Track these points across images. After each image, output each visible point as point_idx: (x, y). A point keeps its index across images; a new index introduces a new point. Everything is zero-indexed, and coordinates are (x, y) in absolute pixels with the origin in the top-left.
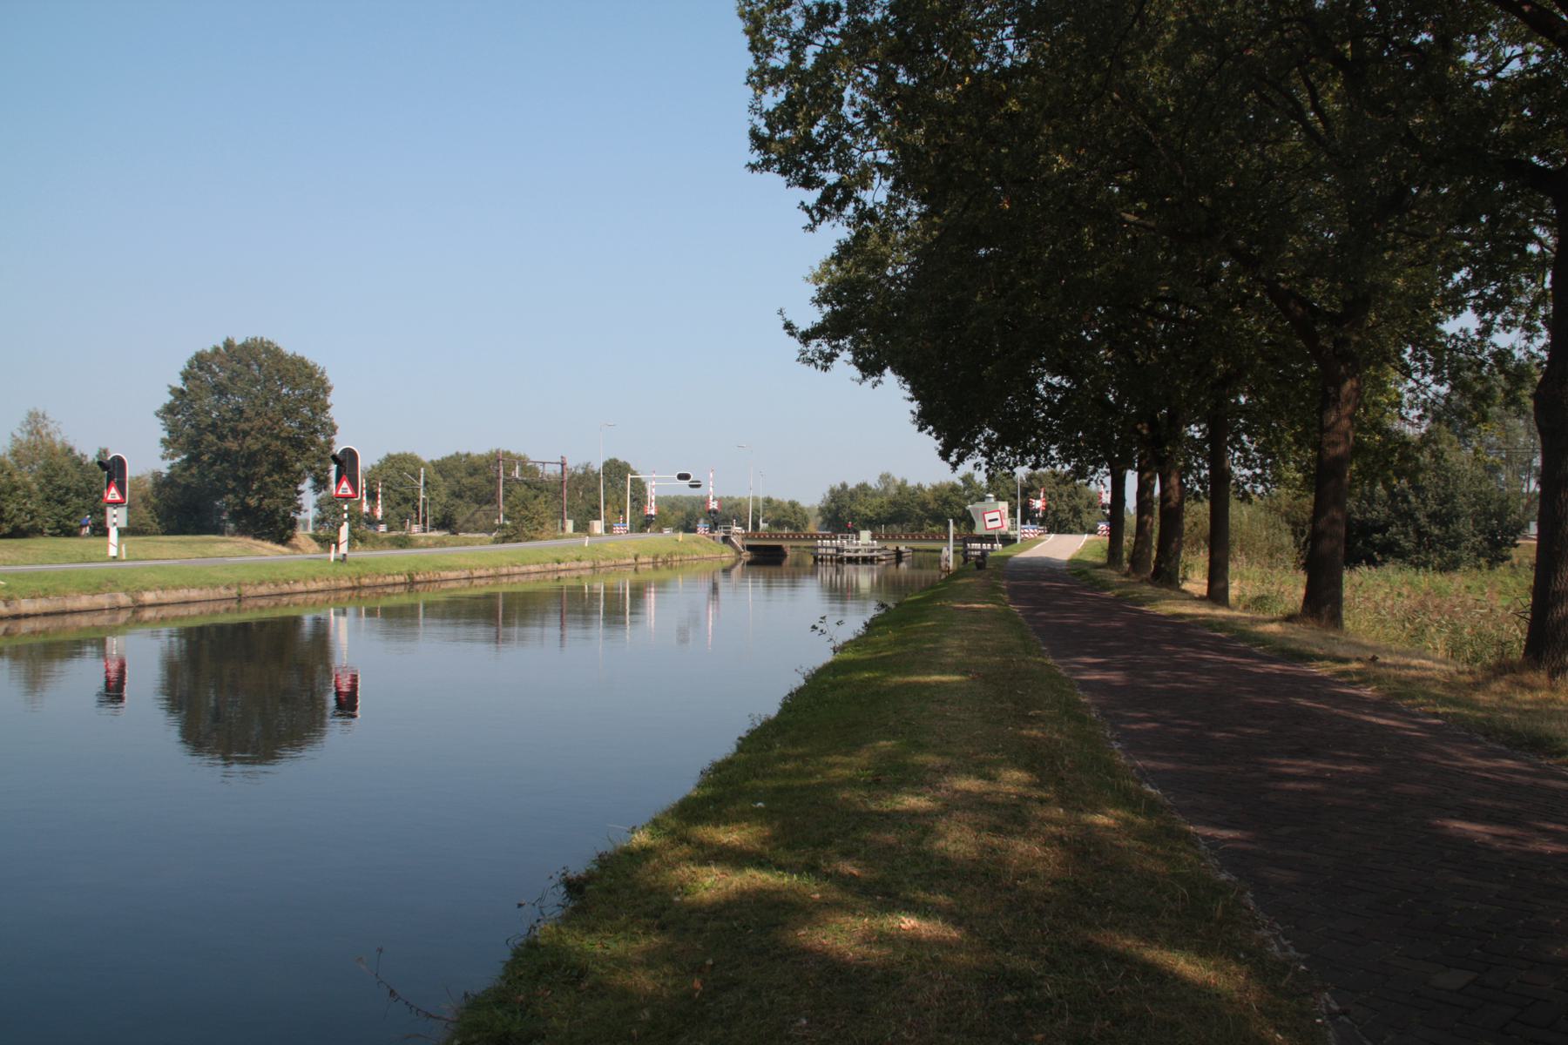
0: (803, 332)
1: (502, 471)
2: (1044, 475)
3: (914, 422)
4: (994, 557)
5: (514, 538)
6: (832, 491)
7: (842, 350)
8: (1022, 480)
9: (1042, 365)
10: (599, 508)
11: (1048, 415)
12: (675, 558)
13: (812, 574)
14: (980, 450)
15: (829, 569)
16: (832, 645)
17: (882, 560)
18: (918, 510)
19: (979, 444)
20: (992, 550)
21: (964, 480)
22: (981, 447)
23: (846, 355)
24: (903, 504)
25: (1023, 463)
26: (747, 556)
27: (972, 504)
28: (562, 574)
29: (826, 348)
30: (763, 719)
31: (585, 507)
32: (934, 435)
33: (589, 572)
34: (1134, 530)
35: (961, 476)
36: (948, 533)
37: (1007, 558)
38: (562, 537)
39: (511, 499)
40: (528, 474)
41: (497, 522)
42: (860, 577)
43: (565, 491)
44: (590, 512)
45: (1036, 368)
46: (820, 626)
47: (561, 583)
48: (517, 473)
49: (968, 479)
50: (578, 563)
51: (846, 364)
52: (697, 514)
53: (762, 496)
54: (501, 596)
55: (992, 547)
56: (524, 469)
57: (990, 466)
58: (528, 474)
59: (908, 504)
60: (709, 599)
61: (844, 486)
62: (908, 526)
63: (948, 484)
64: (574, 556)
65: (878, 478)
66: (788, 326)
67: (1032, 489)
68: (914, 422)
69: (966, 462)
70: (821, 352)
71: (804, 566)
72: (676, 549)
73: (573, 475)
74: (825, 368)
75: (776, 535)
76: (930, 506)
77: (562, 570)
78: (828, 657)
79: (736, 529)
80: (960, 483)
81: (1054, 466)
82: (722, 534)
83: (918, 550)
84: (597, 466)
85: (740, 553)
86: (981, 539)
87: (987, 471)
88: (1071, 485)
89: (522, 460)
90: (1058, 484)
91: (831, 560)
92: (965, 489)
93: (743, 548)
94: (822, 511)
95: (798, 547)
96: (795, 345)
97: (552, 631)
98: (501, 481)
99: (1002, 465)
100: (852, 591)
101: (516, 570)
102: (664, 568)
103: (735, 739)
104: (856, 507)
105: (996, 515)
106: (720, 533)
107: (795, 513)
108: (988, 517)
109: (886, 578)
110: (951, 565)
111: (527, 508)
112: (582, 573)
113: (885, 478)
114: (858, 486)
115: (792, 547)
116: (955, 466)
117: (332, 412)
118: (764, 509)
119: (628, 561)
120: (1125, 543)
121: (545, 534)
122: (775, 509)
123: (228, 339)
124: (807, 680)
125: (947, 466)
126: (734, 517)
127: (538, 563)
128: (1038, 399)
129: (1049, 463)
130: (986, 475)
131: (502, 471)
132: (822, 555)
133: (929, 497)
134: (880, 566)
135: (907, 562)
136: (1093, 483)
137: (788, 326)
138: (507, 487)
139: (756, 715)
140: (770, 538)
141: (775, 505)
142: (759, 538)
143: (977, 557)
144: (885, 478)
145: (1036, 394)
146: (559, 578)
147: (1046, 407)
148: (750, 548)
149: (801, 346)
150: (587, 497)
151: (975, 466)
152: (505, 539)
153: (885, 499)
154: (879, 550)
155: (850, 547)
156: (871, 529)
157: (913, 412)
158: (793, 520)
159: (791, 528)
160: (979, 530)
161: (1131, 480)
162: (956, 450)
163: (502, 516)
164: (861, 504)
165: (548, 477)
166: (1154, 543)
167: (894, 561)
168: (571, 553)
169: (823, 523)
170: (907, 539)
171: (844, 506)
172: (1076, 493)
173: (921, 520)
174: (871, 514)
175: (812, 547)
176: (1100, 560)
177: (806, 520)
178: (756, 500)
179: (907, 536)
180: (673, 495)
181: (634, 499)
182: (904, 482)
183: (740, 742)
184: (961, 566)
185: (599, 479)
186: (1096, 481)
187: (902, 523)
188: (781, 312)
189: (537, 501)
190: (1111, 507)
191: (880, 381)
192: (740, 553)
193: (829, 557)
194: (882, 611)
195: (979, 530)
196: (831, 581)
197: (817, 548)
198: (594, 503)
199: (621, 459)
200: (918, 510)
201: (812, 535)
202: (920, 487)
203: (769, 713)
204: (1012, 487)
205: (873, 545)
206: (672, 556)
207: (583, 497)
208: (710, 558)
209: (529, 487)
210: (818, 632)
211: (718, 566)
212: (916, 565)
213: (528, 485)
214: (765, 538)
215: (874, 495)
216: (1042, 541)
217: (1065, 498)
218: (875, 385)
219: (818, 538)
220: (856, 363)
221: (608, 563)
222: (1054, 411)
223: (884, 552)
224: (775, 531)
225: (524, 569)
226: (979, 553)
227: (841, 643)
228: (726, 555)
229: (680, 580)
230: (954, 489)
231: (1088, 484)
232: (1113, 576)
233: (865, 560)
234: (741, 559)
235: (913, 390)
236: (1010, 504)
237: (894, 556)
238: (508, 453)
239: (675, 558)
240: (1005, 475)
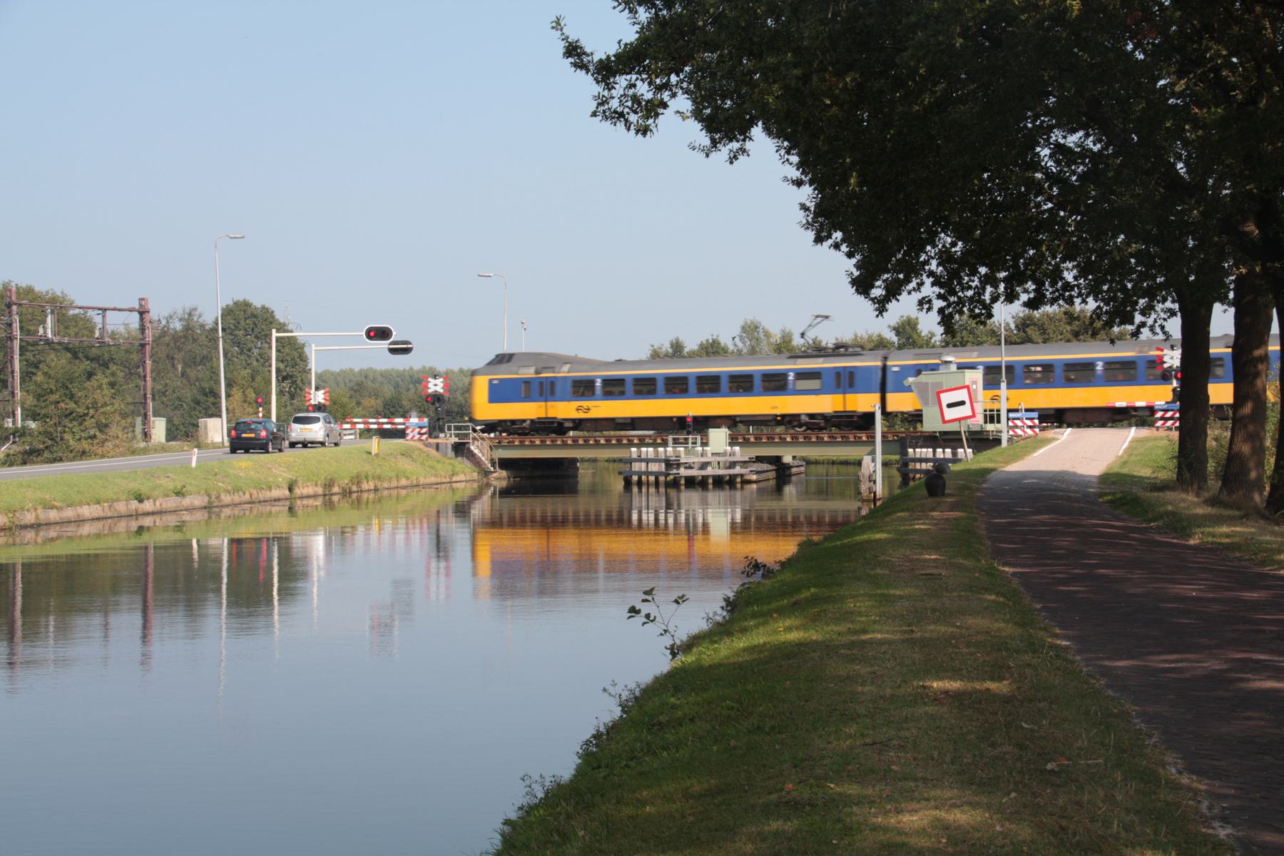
1: (16, 326)
2: (1051, 318)
3: (808, 225)
4: (959, 473)
5: (47, 454)
8: (1007, 328)
9: (1048, 112)
10: (217, 396)
11: (1060, 205)
12: (365, 486)
14: (931, 274)
16: (668, 641)
17: (750, 482)
19: (927, 262)
20: (955, 460)
23: (682, 103)
25: (1011, 297)
26: (500, 478)
28: (147, 522)
29: (644, 91)
30: (547, 784)
31: (188, 394)
35: (894, 322)
38: (145, 451)
39: (39, 378)
40: (72, 332)
41: (9, 423)
44: (198, 403)
45: (1036, 117)
46: (645, 609)
47: (146, 538)
48: (48, 329)
50: (179, 499)
51: (750, 153)
52: (405, 403)
54: (19, 568)
55: (954, 454)
56: (64, 322)
58: (72, 332)
60: (430, 557)
64: (171, 486)
66: (573, 51)
68: (808, 225)
69: (904, 297)
70: (636, 99)
72: (367, 468)
74: (644, 131)
77: (147, 514)
80: (892, 337)
81: (1070, 301)
82: (455, 440)
83: (816, 463)
84: (210, 314)
86: (934, 440)
87: (941, 311)
89: (58, 305)
91: (657, 484)
93: (493, 464)
95: (594, 460)
96: (587, 86)
97: (126, 621)
98: (17, 344)
101: (53, 515)
102: (345, 505)
103: (498, 825)
105: (962, 395)
108: (947, 398)
110: (879, 488)
111: (72, 397)
112: (186, 517)
116: (881, 306)
119: (276, 493)
121: (109, 445)
123: (677, 339)
124: (624, 707)
125: (867, 307)
128: (1039, 175)
129: (1062, 296)
131: (16, 326)
132: (640, 474)
137: (573, 51)
138: (29, 355)
139: (536, 777)
143: (927, 472)
145: (1036, 165)
147: (1055, 191)
148: (505, 464)
149: (598, 89)
150: (192, 373)
151: (921, 303)
152: (29, 457)
154: (744, 464)
155: (691, 460)
157: (804, 207)
161: (1222, 321)
163: (19, 411)
166: (1268, 443)
167: (773, 483)
168: (163, 481)
175: (620, 460)
176: (1164, 475)
180: (357, 369)
181: (282, 378)
183: (507, 829)
185: (216, 340)
186: (1152, 328)
188: (558, 25)
189: (94, 383)
191: (743, 151)
192: (486, 473)
193: (652, 478)
196: (657, 520)
197: (630, 461)
198: (206, 385)
199: (257, 302)
203: (558, 773)
205: (732, 454)
206: (359, 483)
207: (183, 374)
208: (430, 485)
209: (75, 356)
210: (640, 619)
211: (446, 498)
212: (813, 489)
213: (74, 353)
218: (733, 159)
220: (697, 114)
222: (1069, 197)
225: (69, 513)
226: (929, 466)
227: (685, 638)
228: (461, 477)
232: (1189, 502)
234: (488, 485)
238: (29, 291)
239: (365, 486)
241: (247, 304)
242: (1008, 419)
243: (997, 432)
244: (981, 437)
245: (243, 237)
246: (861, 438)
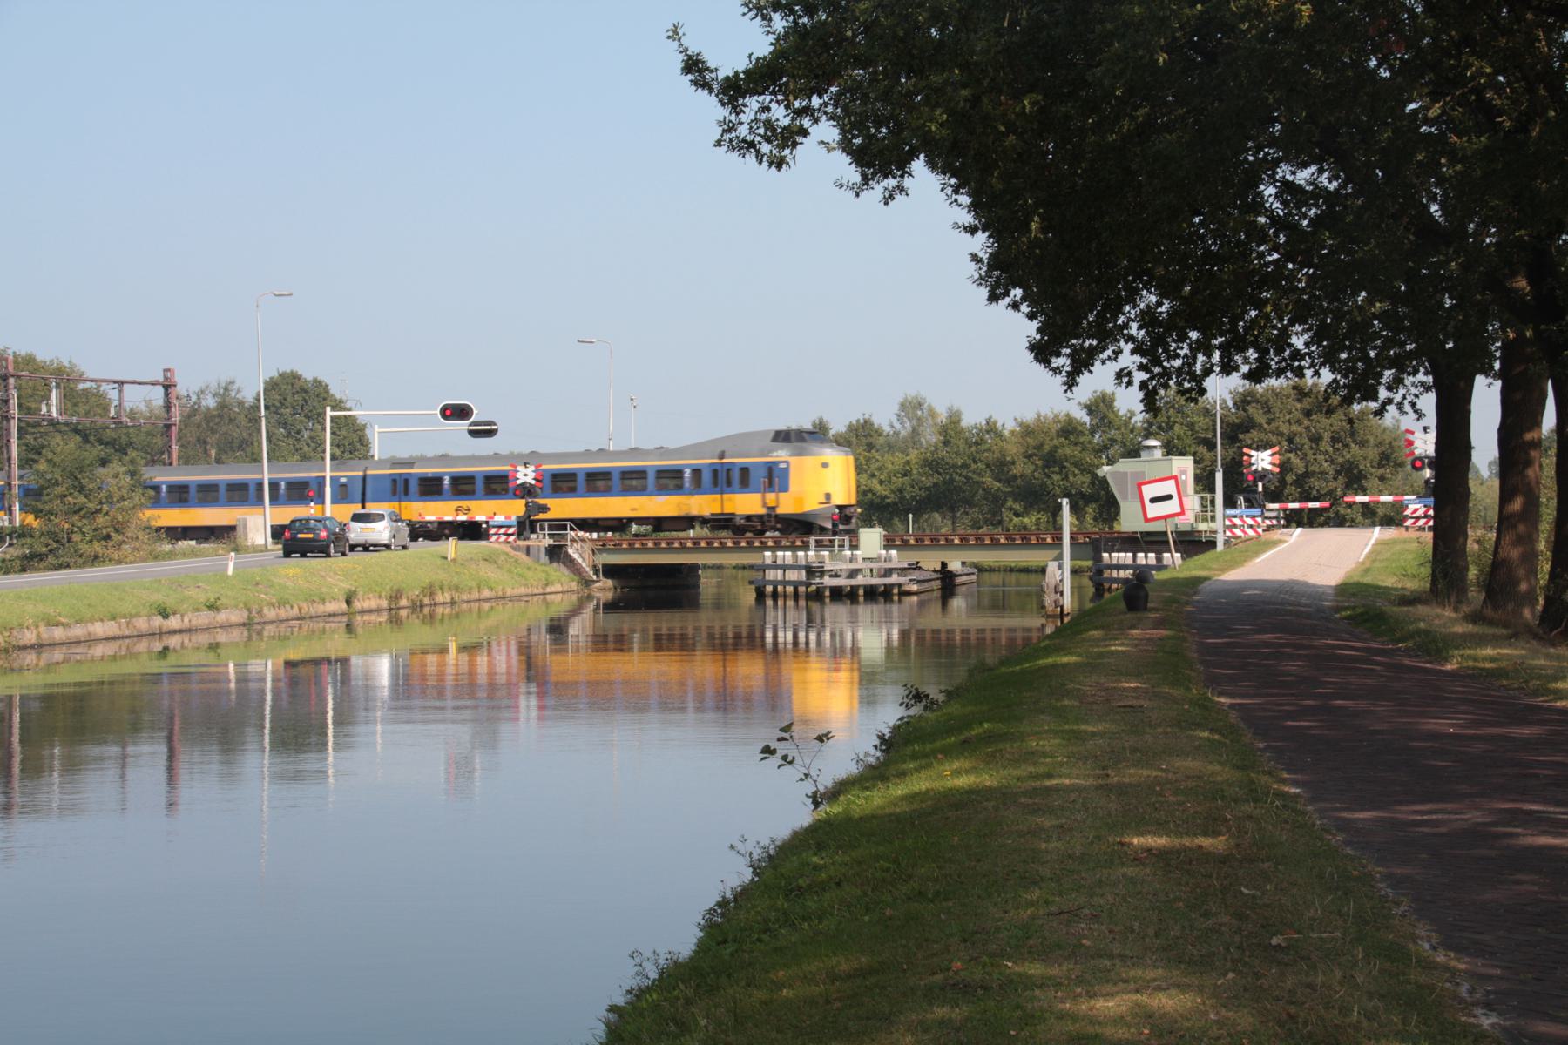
0: (727, 78)
1: (14, 402)
4: (1164, 583)
5: (51, 559)
7: (816, 121)
8: (1224, 406)
11: (1287, 256)
12: (440, 598)
15: (791, 614)
16: (811, 789)
17: (909, 593)
18: (988, 480)
20: (1160, 566)
23: (826, 131)
24: (955, 466)
25: (1228, 368)
26: (605, 589)
27: (1111, 462)
28: (174, 641)
29: (780, 115)
33: (237, 635)
34: (1493, 515)
35: (1084, 400)
37: (1195, 582)
39: (42, 466)
42: (860, 635)
43: (175, 447)
45: (1259, 148)
48: (53, 407)
49: (1100, 407)
55: (1159, 559)
56: (71, 397)
58: (82, 409)
59: (965, 466)
63: (1056, 419)
64: (202, 597)
65: (896, 408)
66: (694, 66)
67: (1247, 425)
70: (769, 125)
72: (442, 576)
73: (194, 411)
74: (779, 163)
78: (803, 816)
80: (1082, 416)
82: (549, 542)
83: (991, 570)
84: (251, 388)
85: (588, 583)
86: (1133, 542)
88: (1339, 415)
89: (65, 378)
90: (1308, 414)
92: (1092, 432)
93: (596, 571)
96: (710, 108)
98: (14, 424)
101: (59, 634)
102: (415, 621)
105: (1168, 487)
108: (1149, 491)
110: (1067, 601)
111: (81, 489)
113: (912, 408)
114: (851, 428)
116: (1071, 383)
117: (1008, 425)
119: (331, 607)
120: (1472, 546)
121: (127, 548)
127: (114, 618)
128: (1262, 220)
129: (1289, 367)
130: (1141, 395)
131: (14, 402)
132: (775, 584)
133: (1013, 450)
135: (966, 596)
136: (1392, 409)
137: (694, 66)
139: (647, 953)
143: (1126, 581)
144: (912, 408)
145: (1258, 206)
146: (166, 649)
148: (610, 571)
149: (723, 113)
151: (1119, 375)
153: (913, 455)
155: (837, 566)
156: (882, 524)
157: (975, 258)
160: (1130, 521)
161: (1486, 400)
165: (132, 414)
167: (937, 594)
168: (193, 592)
172: (1352, 434)
173: (996, 502)
176: (1411, 585)
179: (964, 539)
182: (954, 418)
183: (612, 1017)
184: (1089, 605)
185: (257, 420)
186: (1400, 406)
188: (675, 33)
190: (1434, 463)
191: (901, 189)
192: (588, 583)
193: (790, 589)
195: (1130, 521)
197: (763, 568)
199: (308, 374)
200: (988, 480)
202: (991, 428)
203: (675, 949)
204: (1202, 422)
206: (432, 594)
209: (86, 439)
210: (775, 761)
211: (539, 615)
213: (84, 435)
215: (891, 447)
216: (1281, 541)
217: (1325, 446)
218: (888, 198)
220: (846, 145)
221: (283, 614)
222: (1300, 246)
223: (916, 575)
225: (78, 631)
226: (1129, 574)
227: (830, 784)
228: (558, 588)
230: (1069, 429)
231: (1380, 412)
232: (1445, 618)
234: (590, 597)
235: (974, 207)
237: (937, 585)
238: (30, 360)
239: (440, 598)
241: (295, 377)
242: (1225, 517)
244: (1191, 539)
245: (291, 295)
246: (1045, 539)
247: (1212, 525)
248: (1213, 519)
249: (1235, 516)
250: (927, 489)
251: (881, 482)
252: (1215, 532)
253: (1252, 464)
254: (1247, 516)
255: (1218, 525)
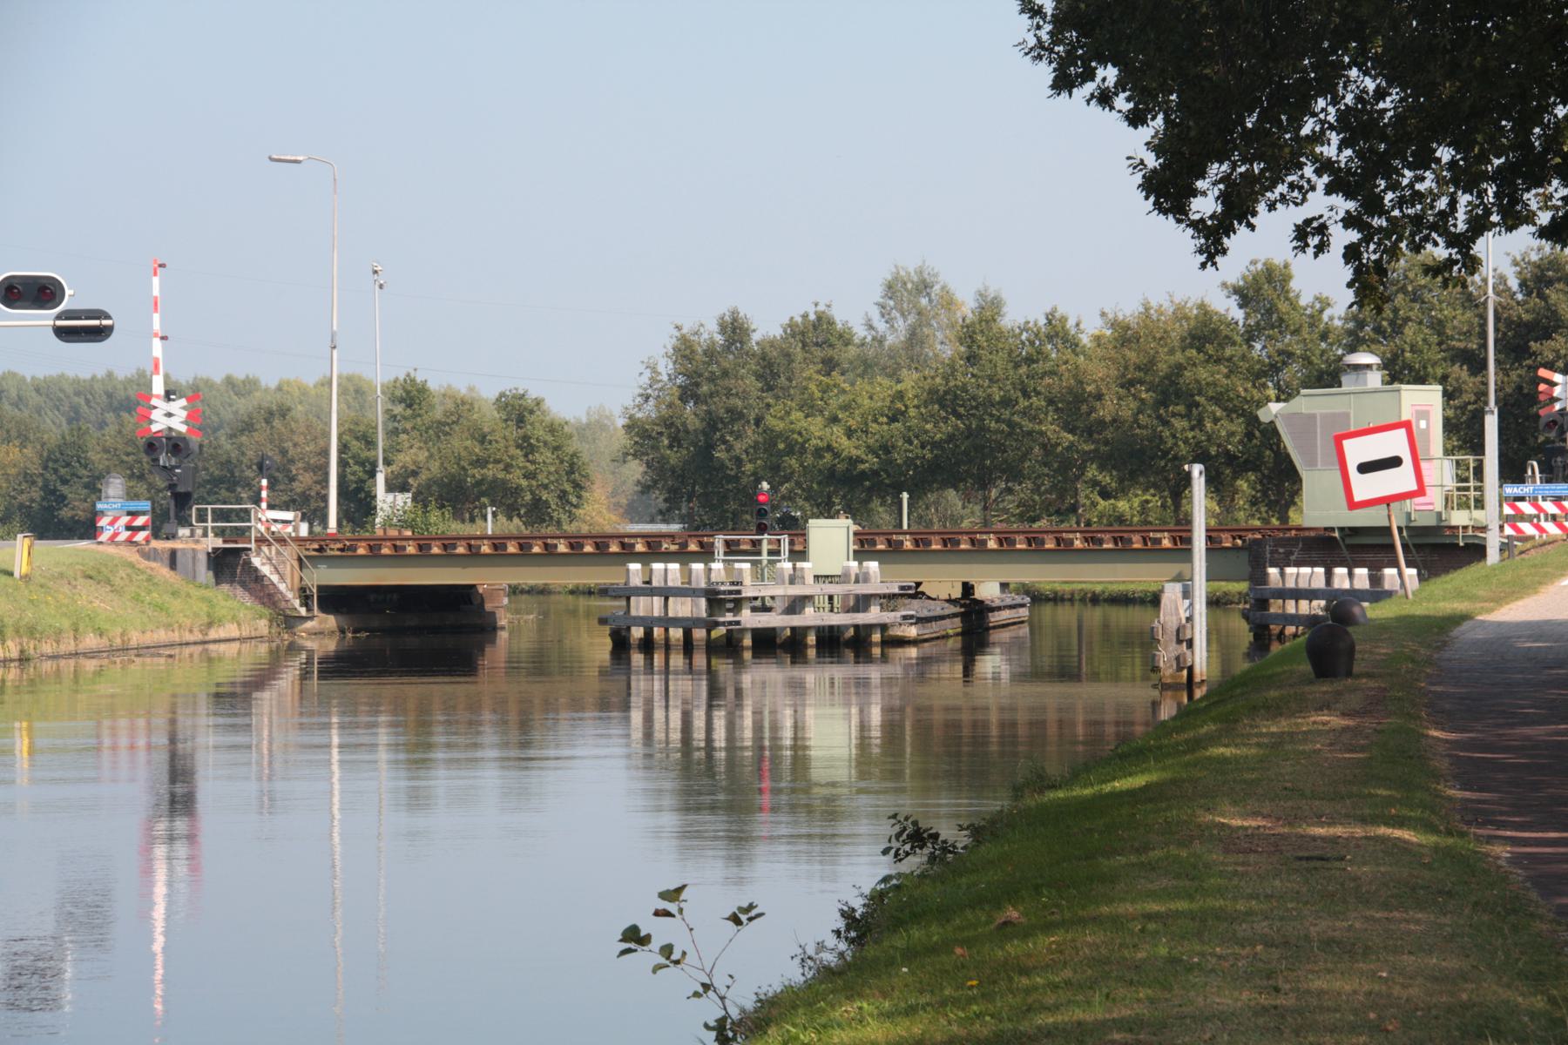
6: (685, 351)
13: (604, 705)
14: (1325, 166)
16: (710, 1010)
17: (902, 642)
18: (1051, 428)
19: (1318, 138)
20: (1377, 593)
21: (1246, 295)
22: (1330, 151)
25: (1514, 218)
32: (1122, 103)
36: (1187, 522)
37: (1441, 627)
46: (663, 929)
52: (94, 456)
53: (381, 373)
55: (1376, 580)
57: (1368, 233)
59: (1007, 402)
61: (735, 329)
62: (1009, 498)
63: (1180, 314)
65: (877, 294)
69: (1262, 216)
71: (570, 667)
75: (448, 544)
76: (1106, 411)
79: (268, 518)
83: (1056, 599)
85: (289, 621)
87: (1351, 253)
91: (688, 646)
93: (306, 600)
94: (642, 436)
95: (543, 591)
99: (1422, 228)
100: (776, 775)
104: (787, 418)
105: (1393, 443)
106: (198, 540)
107: (527, 446)
108: (1358, 450)
109: (923, 730)
110: (1200, 658)
115: (514, 591)
116: (1213, 239)
118: (393, 433)
122: (441, 429)
126: (261, 468)
130: (1347, 273)
132: (648, 624)
133: (1098, 372)
134: (894, 670)
135: (1010, 648)
140: (424, 556)
141: (438, 414)
142: (374, 556)
143: (1312, 621)
148: (333, 599)
153: (910, 381)
154: (889, 600)
156: (851, 512)
158: (516, 478)
159: (511, 511)
162: (1216, 169)
164: (809, 408)
167: (955, 644)
169: (646, 489)
170: (1006, 549)
171: (736, 415)
173: (1066, 468)
174: (847, 446)
177: (574, 477)
178: (355, 390)
179: (1005, 540)
182: (990, 309)
187: (984, 483)
193: (676, 634)
194: (914, 863)
197: (627, 594)
200: (1051, 428)
201: (601, 542)
202: (1056, 331)
204: (1461, 318)
205: (862, 578)
210: (647, 957)
211: (190, 676)
212: (1046, 662)
214: (399, 557)
215: (866, 367)
219: (628, 553)
223: (914, 608)
224: (442, 523)
226: (1318, 606)
227: (750, 1005)
228: (231, 630)
229: (22, 745)
233: (832, 643)
234: (293, 649)
236: (1448, 396)
240: (1438, 270)
243: (1475, 528)
246: (1159, 541)
247: (1478, 515)
248: (1480, 504)
249: (1522, 499)
250: (935, 445)
251: (850, 433)
252: (1484, 529)
253: (1554, 400)
254: (1544, 499)
255: (1489, 515)
